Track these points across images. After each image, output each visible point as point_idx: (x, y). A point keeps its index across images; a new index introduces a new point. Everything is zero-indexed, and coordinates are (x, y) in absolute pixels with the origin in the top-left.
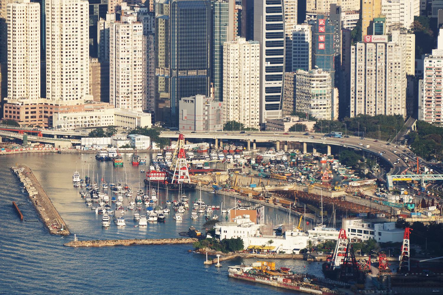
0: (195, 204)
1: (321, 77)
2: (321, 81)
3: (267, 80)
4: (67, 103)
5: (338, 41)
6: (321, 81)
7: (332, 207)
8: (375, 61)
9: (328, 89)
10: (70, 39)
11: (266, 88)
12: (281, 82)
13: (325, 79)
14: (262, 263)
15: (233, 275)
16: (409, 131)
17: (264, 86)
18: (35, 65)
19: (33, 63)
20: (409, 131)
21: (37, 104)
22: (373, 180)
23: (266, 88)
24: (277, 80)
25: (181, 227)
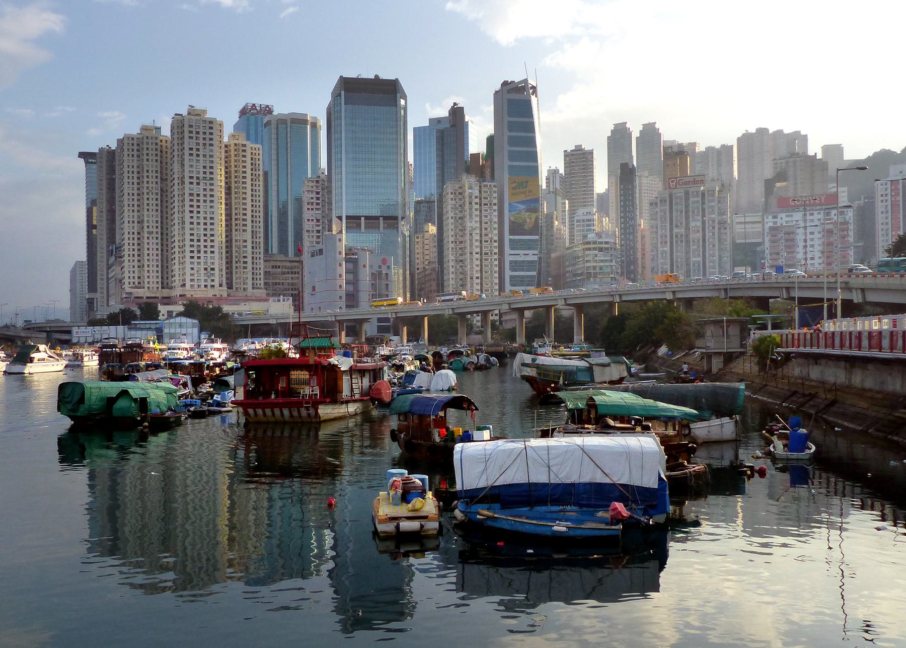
0: (251, 455)
1: (601, 243)
2: (601, 250)
3: (512, 248)
4: (192, 293)
5: (631, 215)
6: (601, 250)
7: (528, 146)
8: (704, 206)
9: (613, 263)
10: (198, 195)
11: (511, 262)
12: (536, 252)
13: (606, 246)
14: (850, 380)
15: (863, 404)
16: (807, 315)
17: (508, 259)
18: (155, 233)
19: (151, 230)
20: (807, 315)
21: (160, 298)
22: (497, 598)
23: (511, 262)
24: (529, 249)
25: (851, 514)
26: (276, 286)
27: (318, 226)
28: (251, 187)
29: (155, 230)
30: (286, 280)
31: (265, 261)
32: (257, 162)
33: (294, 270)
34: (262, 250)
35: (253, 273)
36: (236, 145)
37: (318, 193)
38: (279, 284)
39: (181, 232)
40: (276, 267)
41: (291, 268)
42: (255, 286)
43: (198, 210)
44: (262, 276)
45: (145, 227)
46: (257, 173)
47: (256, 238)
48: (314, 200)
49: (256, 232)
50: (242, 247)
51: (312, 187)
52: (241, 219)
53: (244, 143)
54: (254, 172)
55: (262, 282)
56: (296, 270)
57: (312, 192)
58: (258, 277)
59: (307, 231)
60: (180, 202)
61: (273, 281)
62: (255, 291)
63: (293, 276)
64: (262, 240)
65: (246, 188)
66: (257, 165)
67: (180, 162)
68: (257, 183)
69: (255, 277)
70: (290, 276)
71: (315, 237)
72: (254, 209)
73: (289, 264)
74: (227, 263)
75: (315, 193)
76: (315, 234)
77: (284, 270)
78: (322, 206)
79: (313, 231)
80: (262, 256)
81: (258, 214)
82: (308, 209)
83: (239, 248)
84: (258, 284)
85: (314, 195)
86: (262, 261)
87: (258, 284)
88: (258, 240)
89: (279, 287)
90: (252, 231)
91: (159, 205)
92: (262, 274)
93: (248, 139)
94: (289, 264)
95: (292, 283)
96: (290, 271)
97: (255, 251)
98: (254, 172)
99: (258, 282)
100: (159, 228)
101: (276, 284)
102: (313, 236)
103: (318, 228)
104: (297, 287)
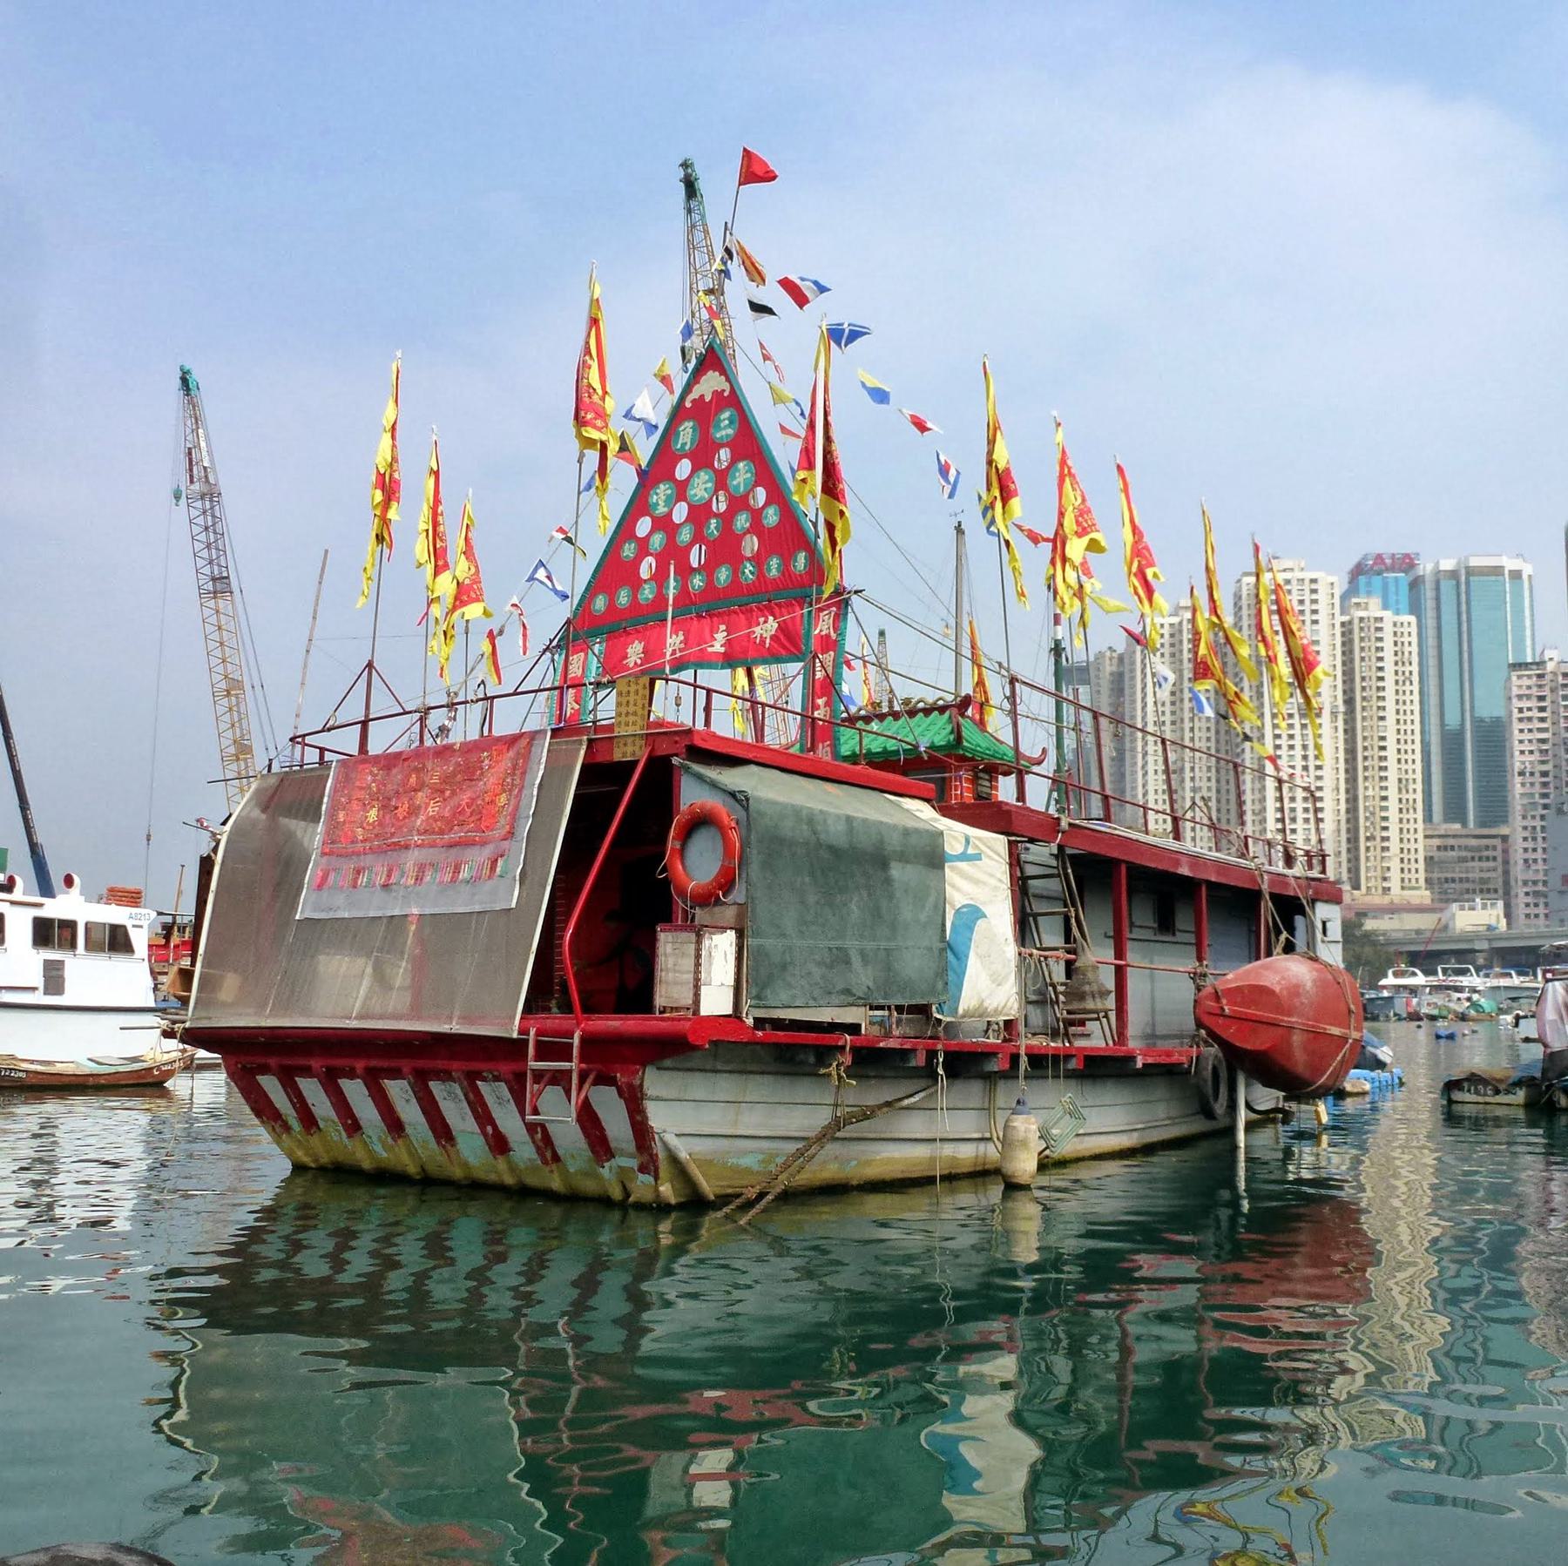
26: (1446, 885)
27: (1543, 762)
28: (1395, 688)
29: (1204, 784)
30: (1467, 872)
31: (1426, 837)
32: (1407, 649)
33: (1486, 853)
34: (1420, 815)
35: (1402, 860)
36: (1361, 619)
37: (1542, 698)
38: (1453, 880)
39: (1258, 786)
40: (1445, 848)
41: (1479, 849)
42: (1406, 883)
43: (1291, 742)
44: (1421, 866)
45: (1187, 780)
46: (1407, 668)
47: (1407, 791)
48: (1535, 691)
49: (1407, 780)
50: (1378, 809)
51: (1529, 687)
52: (1376, 757)
53: (1379, 614)
54: (1400, 668)
55: (1422, 876)
56: (1490, 853)
57: (1529, 697)
58: (1409, 717)
59: (1521, 774)
60: (1256, 792)
61: (1440, 875)
62: (1406, 892)
63: (1485, 864)
64: (1419, 797)
65: (1386, 778)
66: (1406, 654)
67: (1254, 689)
68: (1408, 688)
69: (1406, 875)
70: (1476, 864)
71: (1537, 786)
72: (1403, 757)
73: (1474, 842)
74: (1349, 840)
75: (1535, 699)
76: (1538, 779)
77: (1464, 854)
78: (1554, 724)
79: (1532, 774)
80: (1420, 826)
81: (1409, 747)
82: (1522, 752)
83: (1373, 814)
84: (1413, 881)
85: (1533, 703)
86: (1420, 836)
87: (1413, 881)
88: (1411, 796)
89: (1453, 885)
90: (1400, 780)
91: (1213, 739)
92: (1421, 861)
93: (1385, 607)
94: (1474, 842)
95: (1481, 879)
96: (1477, 855)
97: (1405, 816)
98: (1400, 668)
99: (1413, 876)
100: (1214, 780)
101: (1447, 880)
102: (1532, 784)
103: (1544, 768)
104: (1492, 886)
